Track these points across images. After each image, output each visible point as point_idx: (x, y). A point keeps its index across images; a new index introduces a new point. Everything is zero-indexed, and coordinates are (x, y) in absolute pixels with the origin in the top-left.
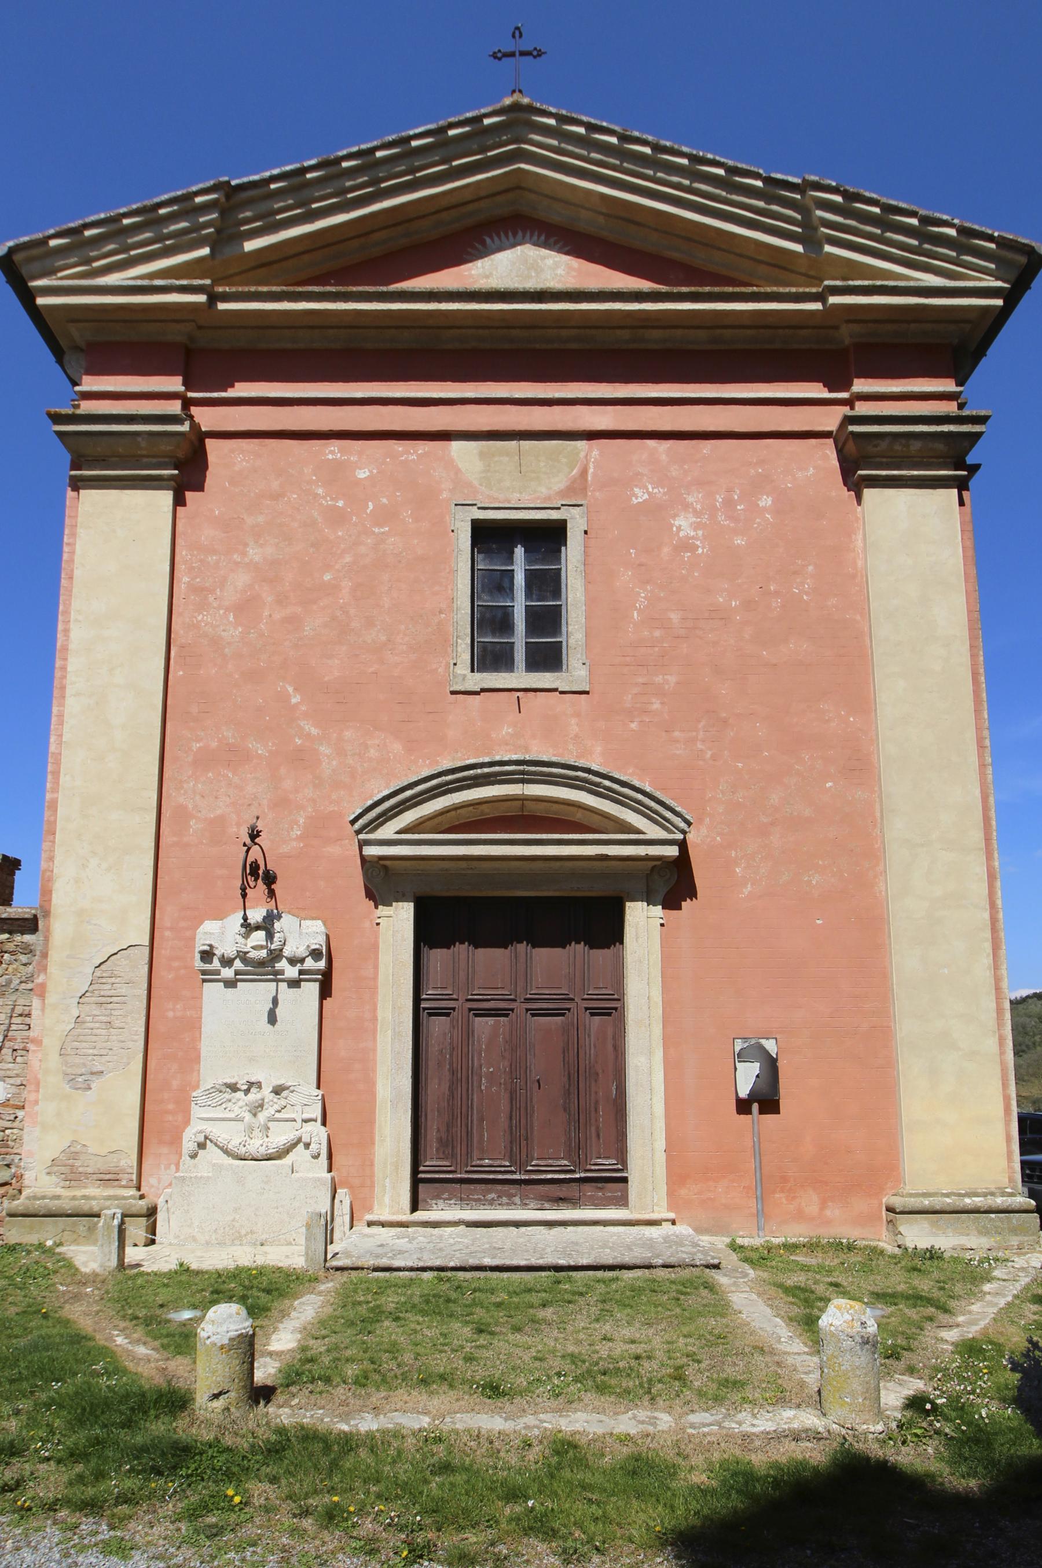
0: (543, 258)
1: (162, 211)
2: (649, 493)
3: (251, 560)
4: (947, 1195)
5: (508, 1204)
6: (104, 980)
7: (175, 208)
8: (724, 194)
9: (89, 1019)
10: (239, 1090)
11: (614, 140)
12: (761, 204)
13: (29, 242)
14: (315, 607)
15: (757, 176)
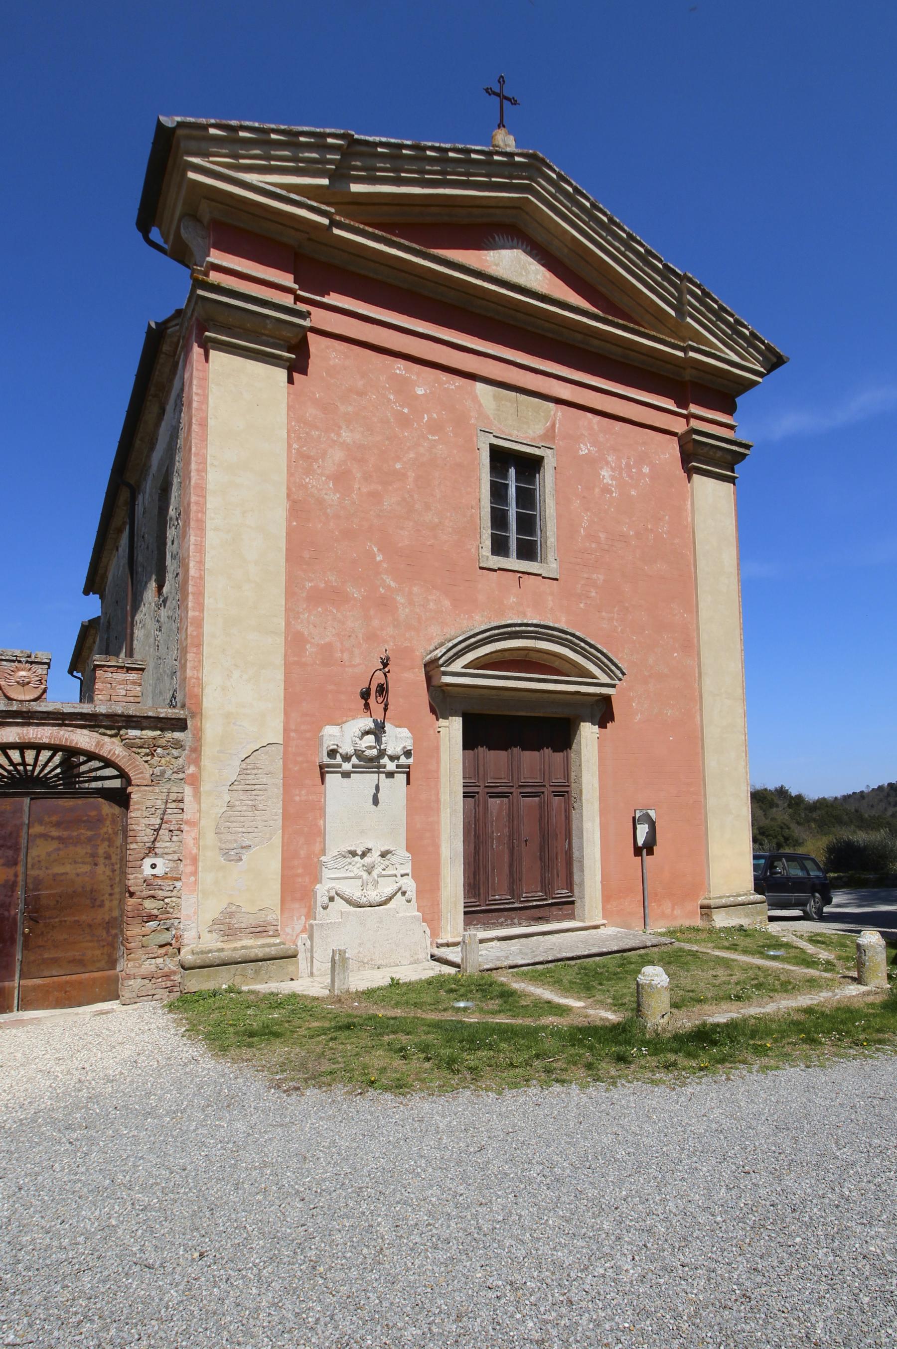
0: (530, 264)
1: (302, 139)
2: (589, 450)
3: (344, 441)
4: (728, 897)
5: (511, 924)
6: (248, 772)
7: (312, 140)
8: (641, 264)
9: (237, 803)
10: (357, 855)
11: (588, 204)
12: (659, 279)
13: (194, 123)
14: (390, 488)
15: (660, 261)
